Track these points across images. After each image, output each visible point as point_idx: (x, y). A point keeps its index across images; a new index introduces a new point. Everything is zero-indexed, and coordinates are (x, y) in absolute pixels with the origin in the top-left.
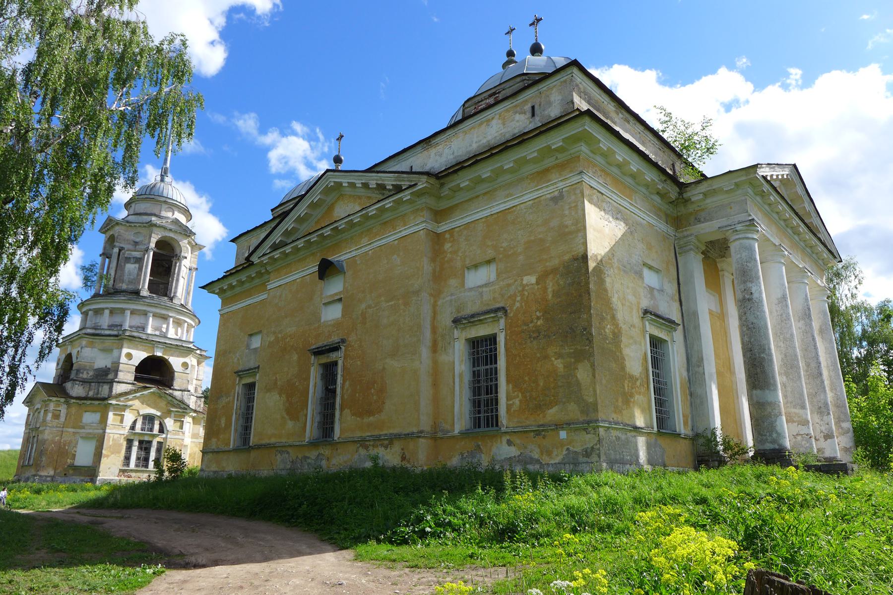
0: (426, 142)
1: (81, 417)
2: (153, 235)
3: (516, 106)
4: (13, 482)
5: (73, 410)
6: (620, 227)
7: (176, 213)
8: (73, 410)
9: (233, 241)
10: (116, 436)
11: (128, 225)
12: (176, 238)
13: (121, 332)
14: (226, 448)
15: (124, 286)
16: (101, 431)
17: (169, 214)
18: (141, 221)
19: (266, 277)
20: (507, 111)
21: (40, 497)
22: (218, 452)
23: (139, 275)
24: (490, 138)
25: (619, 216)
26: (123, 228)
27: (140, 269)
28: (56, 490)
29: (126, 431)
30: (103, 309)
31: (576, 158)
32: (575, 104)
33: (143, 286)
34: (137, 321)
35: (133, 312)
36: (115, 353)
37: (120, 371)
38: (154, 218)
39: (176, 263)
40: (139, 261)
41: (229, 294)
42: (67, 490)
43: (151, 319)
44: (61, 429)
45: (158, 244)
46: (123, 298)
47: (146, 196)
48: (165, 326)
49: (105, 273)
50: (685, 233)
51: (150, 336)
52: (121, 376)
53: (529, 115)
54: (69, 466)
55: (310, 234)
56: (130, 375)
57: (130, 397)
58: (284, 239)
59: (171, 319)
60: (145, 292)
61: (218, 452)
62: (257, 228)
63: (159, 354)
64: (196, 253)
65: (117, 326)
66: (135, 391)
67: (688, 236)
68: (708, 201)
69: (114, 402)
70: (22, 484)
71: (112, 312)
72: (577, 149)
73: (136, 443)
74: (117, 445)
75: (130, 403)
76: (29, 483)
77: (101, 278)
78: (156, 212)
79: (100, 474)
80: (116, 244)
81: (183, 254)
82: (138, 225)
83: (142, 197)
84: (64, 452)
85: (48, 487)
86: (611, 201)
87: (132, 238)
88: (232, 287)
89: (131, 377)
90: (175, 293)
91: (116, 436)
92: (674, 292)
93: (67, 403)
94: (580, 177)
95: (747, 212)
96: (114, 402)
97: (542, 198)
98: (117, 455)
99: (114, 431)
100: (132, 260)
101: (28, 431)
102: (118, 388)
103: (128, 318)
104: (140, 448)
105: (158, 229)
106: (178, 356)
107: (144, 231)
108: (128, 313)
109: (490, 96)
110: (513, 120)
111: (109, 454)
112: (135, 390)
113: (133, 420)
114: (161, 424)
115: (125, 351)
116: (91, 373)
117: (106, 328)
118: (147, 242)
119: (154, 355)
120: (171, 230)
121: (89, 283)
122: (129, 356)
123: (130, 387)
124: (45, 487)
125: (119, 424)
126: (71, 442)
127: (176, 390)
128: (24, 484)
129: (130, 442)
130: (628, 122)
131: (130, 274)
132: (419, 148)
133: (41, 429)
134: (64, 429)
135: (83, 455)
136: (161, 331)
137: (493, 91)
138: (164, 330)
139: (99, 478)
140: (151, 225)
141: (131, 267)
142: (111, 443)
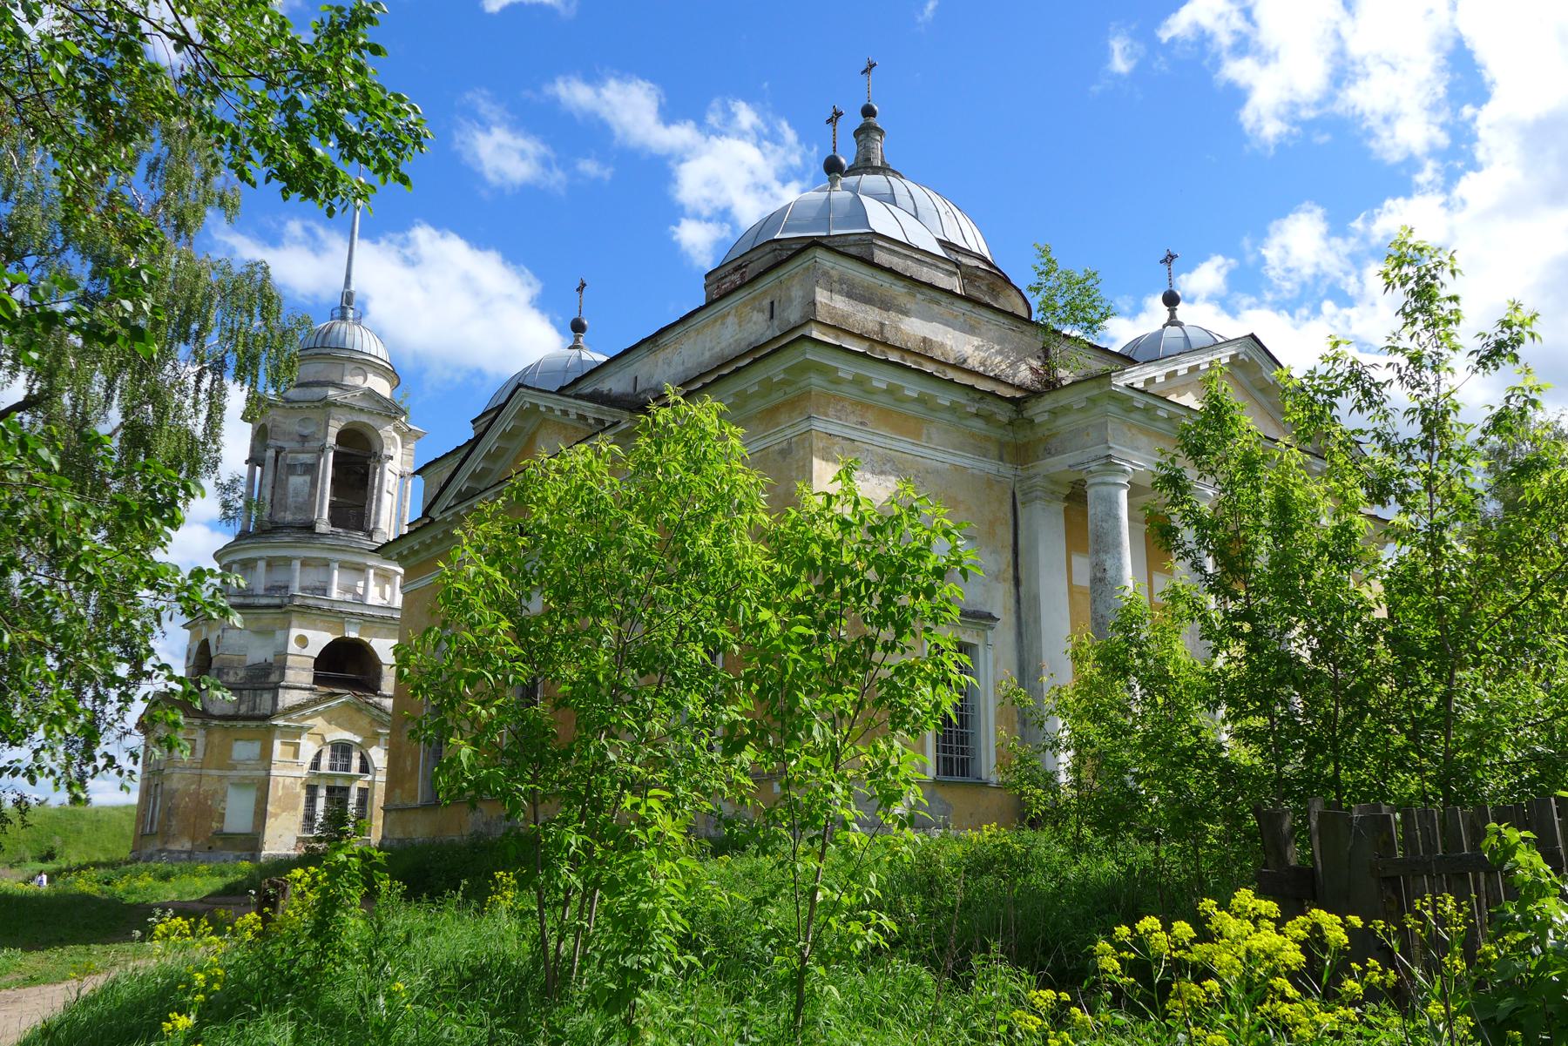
0: (652, 341)
1: (230, 749)
2: (331, 422)
3: (754, 298)
4: (127, 863)
5: (217, 738)
6: (889, 484)
7: (371, 377)
8: (217, 738)
9: (418, 472)
10: (288, 781)
11: (288, 406)
12: (371, 423)
13: (286, 600)
14: (414, 805)
15: (289, 517)
16: (263, 773)
17: (358, 381)
18: (309, 398)
19: (446, 543)
20: (745, 304)
21: (168, 886)
22: (403, 810)
23: (312, 495)
24: (724, 344)
25: (888, 467)
26: (280, 411)
27: (314, 484)
28: (194, 873)
29: (304, 772)
30: (255, 560)
31: (805, 395)
32: (818, 305)
33: (320, 516)
34: (313, 577)
35: (305, 563)
36: (279, 635)
37: (290, 668)
38: (331, 392)
39: (375, 469)
40: (311, 469)
41: (413, 561)
42: (211, 874)
43: (336, 573)
44: (198, 772)
45: (342, 436)
46: (287, 539)
47: (316, 351)
48: (361, 584)
49: (255, 497)
50: (1032, 472)
51: (336, 605)
52: (291, 677)
53: (767, 314)
54: (214, 833)
55: (500, 482)
56: (305, 674)
57: (308, 712)
58: (474, 485)
59: (372, 571)
60: (323, 526)
61: (403, 810)
62: (447, 454)
63: (353, 635)
64: (412, 446)
65: (280, 588)
66: (316, 702)
67: (1029, 478)
68: (1061, 422)
69: (281, 722)
70: (141, 865)
71: (271, 563)
72: (806, 382)
73: (323, 792)
74: (290, 796)
75: (309, 722)
76: (152, 864)
77: (248, 504)
78: (334, 377)
79: (266, 847)
80: (271, 442)
81: (385, 452)
82: (304, 405)
83: (308, 352)
84: (205, 810)
85: (181, 869)
86: (871, 448)
87: (296, 428)
88: (413, 552)
89: (307, 678)
90: (376, 522)
91: (288, 781)
92: (1004, 567)
93: (205, 726)
94: (807, 424)
95: (1106, 442)
96: (281, 722)
97: (771, 449)
98: (292, 813)
99: (284, 773)
100: (299, 470)
101: (146, 776)
102: (288, 698)
103: (298, 574)
104: (329, 799)
105: (339, 411)
106: (386, 637)
107: (316, 415)
108: (297, 564)
109: (736, 270)
110: (750, 321)
111: (279, 811)
112: (315, 700)
113: (315, 752)
114: (363, 758)
115: (295, 632)
116: (242, 673)
117: (262, 592)
118: (321, 435)
119: (344, 638)
120: (361, 410)
121: (230, 513)
122: (303, 641)
123: (305, 695)
124: (176, 869)
125: (291, 759)
126: (216, 792)
127: (386, 696)
128: (144, 865)
129: (312, 791)
130: (938, 303)
131: (297, 495)
132: (644, 348)
133: (166, 772)
134: (204, 771)
135: (237, 817)
136: (355, 593)
137: (739, 262)
138: (360, 591)
139: (263, 853)
140: (327, 404)
141: (297, 482)
142: (280, 793)
